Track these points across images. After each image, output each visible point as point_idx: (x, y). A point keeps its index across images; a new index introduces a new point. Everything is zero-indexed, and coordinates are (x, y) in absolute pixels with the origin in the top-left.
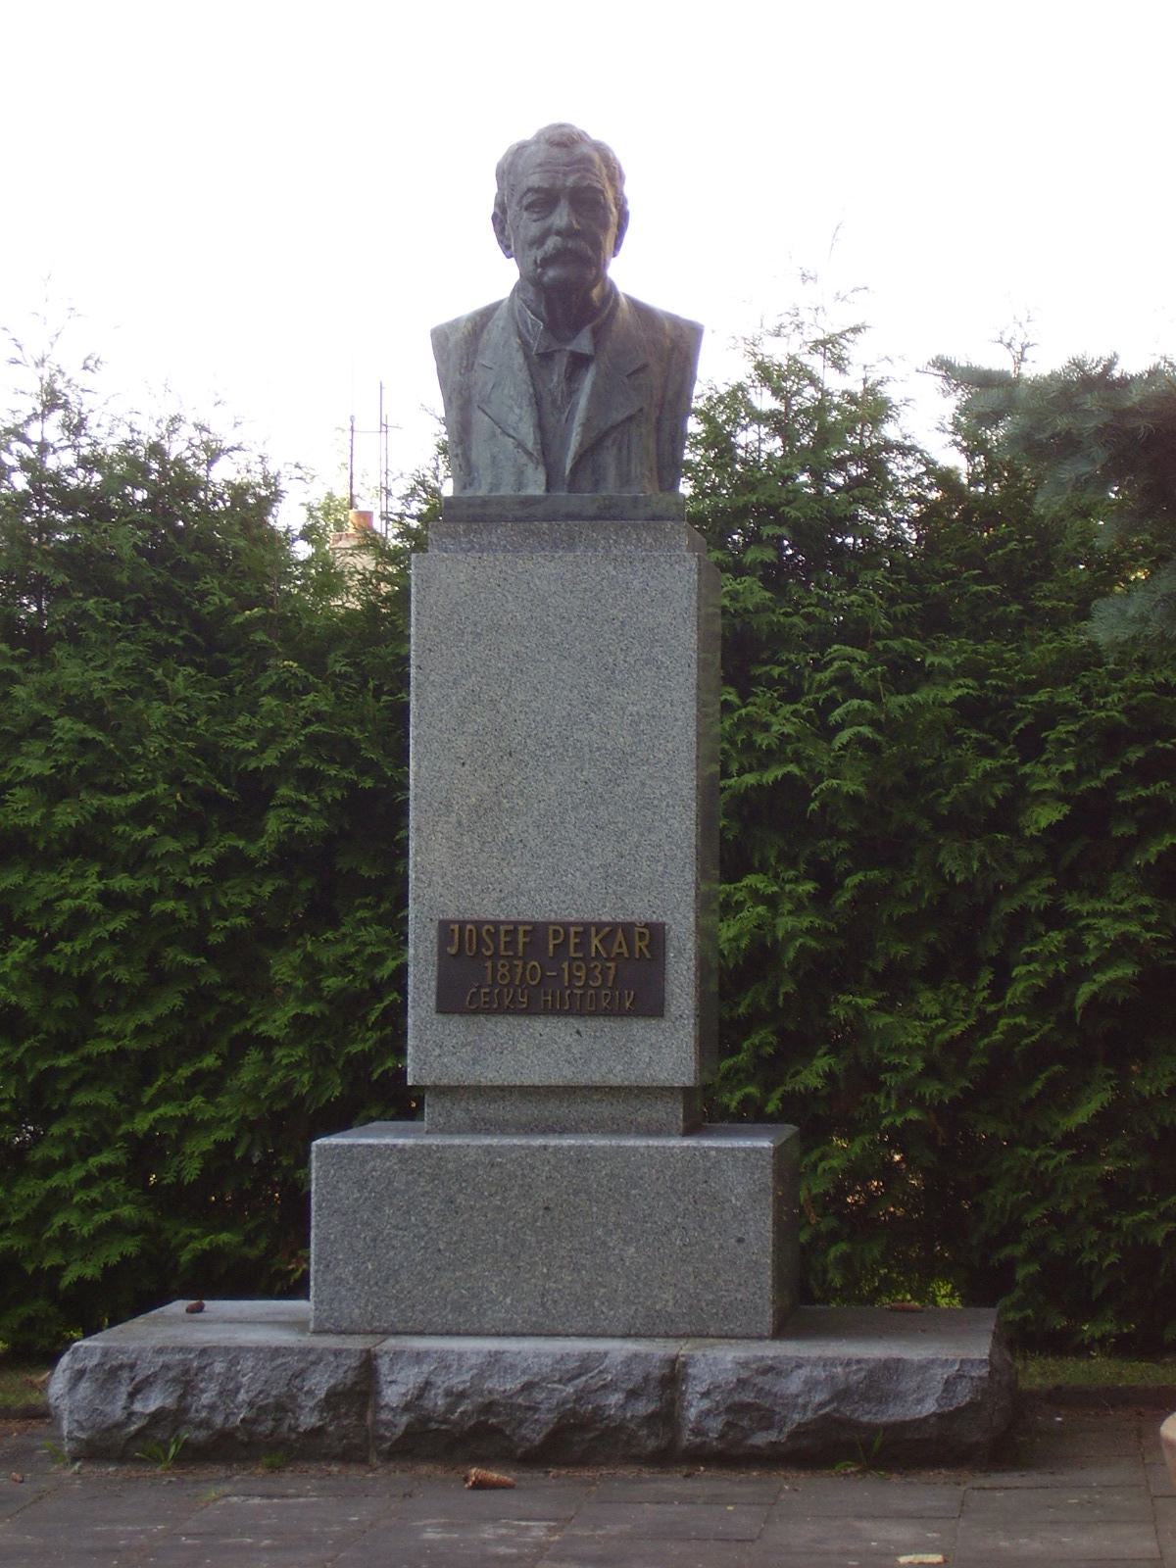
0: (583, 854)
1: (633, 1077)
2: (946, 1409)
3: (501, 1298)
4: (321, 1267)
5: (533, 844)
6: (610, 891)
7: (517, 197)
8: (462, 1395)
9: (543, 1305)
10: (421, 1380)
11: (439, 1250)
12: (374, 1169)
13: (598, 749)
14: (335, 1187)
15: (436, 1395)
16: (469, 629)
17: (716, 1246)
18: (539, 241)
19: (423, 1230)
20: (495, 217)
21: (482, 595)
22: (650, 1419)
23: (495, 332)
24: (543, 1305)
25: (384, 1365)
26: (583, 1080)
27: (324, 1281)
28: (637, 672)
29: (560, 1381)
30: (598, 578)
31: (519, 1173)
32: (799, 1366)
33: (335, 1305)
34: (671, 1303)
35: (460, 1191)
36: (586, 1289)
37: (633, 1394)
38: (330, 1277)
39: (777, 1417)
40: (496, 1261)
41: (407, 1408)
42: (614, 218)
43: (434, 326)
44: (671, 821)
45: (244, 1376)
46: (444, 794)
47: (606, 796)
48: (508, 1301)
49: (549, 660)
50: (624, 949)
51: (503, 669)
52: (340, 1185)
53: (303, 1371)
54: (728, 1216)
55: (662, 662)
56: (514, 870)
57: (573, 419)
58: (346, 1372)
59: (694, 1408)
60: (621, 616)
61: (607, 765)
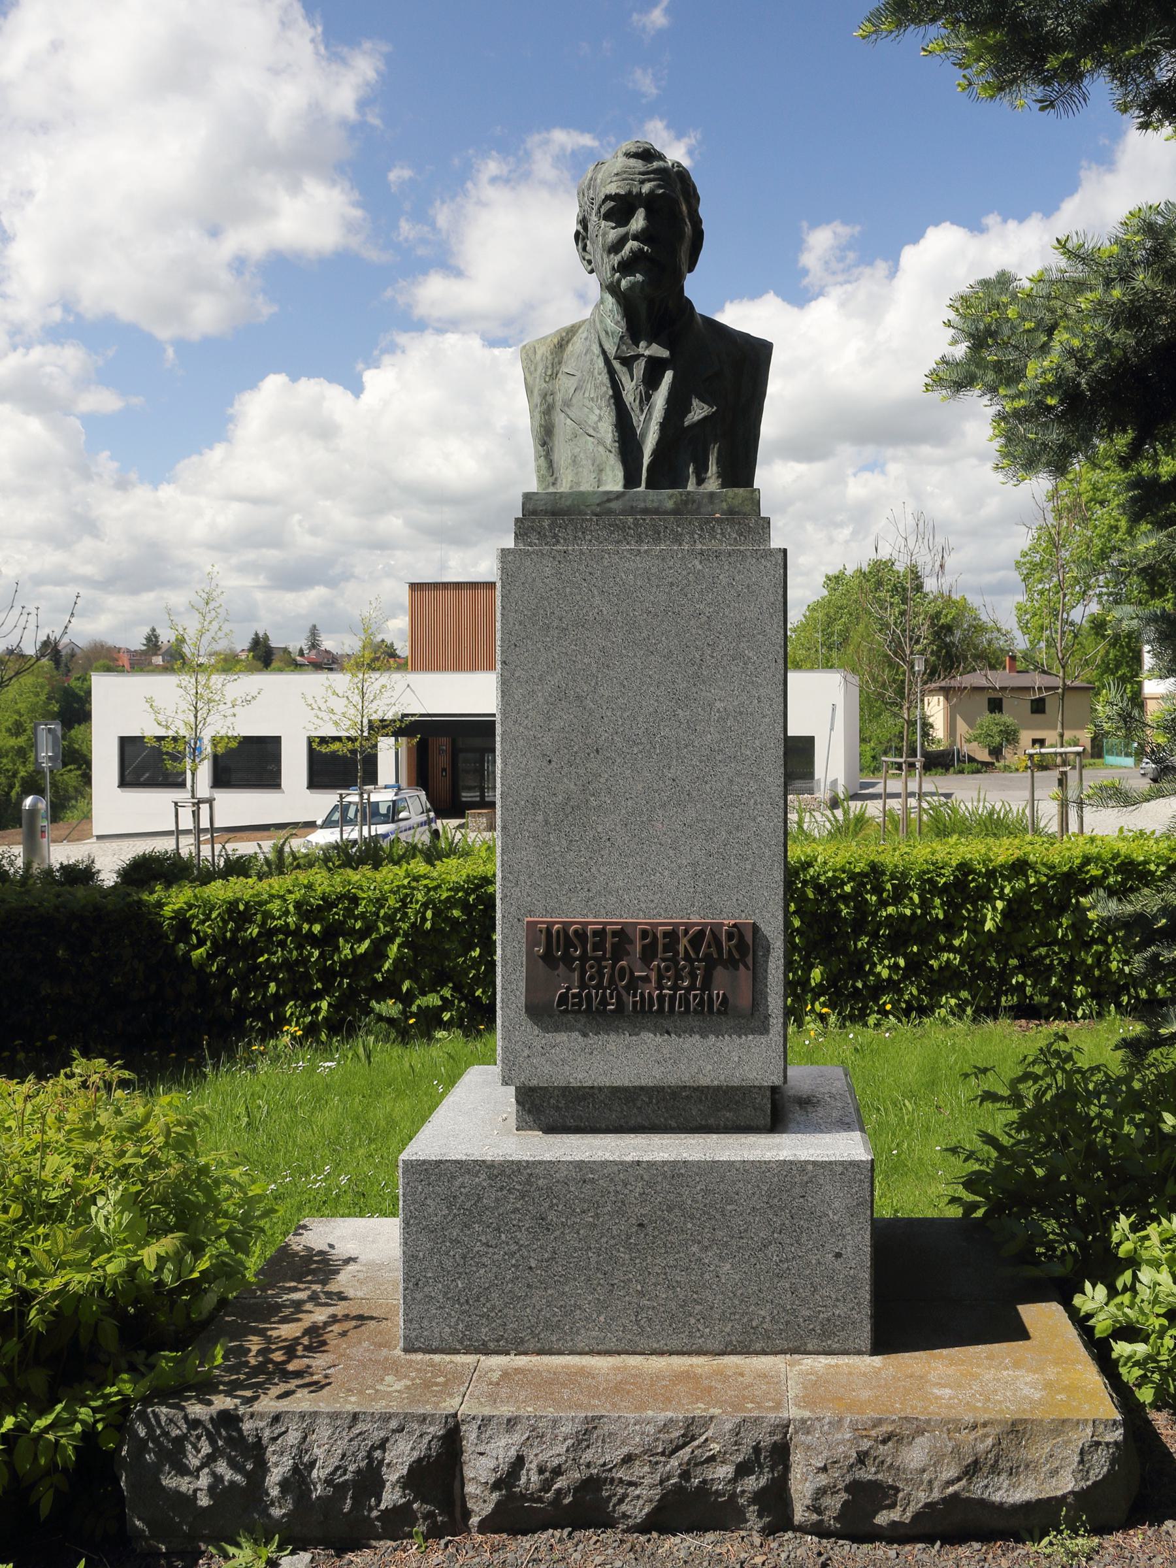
0: (671, 853)
3: (594, 1316)
4: (411, 1285)
5: (620, 842)
6: (699, 890)
7: (595, 207)
8: (557, 1471)
10: (513, 1453)
11: (531, 1268)
12: (462, 1186)
16: (555, 624)
17: (814, 1262)
18: (616, 248)
19: (514, 1248)
20: (577, 234)
21: (568, 590)
25: (470, 1434)
27: (414, 1299)
28: (724, 668)
29: (663, 1454)
30: (684, 573)
31: (612, 1189)
32: (920, 1432)
33: (425, 1323)
34: (768, 1319)
35: (551, 1207)
36: (681, 1306)
38: (419, 1296)
42: (688, 229)
45: (319, 1447)
47: (694, 794)
48: (602, 1319)
49: (635, 655)
51: (590, 664)
52: (428, 1202)
53: (386, 1440)
54: (824, 1230)
55: (749, 658)
56: (603, 870)
57: (650, 419)
58: (430, 1442)
60: (708, 610)
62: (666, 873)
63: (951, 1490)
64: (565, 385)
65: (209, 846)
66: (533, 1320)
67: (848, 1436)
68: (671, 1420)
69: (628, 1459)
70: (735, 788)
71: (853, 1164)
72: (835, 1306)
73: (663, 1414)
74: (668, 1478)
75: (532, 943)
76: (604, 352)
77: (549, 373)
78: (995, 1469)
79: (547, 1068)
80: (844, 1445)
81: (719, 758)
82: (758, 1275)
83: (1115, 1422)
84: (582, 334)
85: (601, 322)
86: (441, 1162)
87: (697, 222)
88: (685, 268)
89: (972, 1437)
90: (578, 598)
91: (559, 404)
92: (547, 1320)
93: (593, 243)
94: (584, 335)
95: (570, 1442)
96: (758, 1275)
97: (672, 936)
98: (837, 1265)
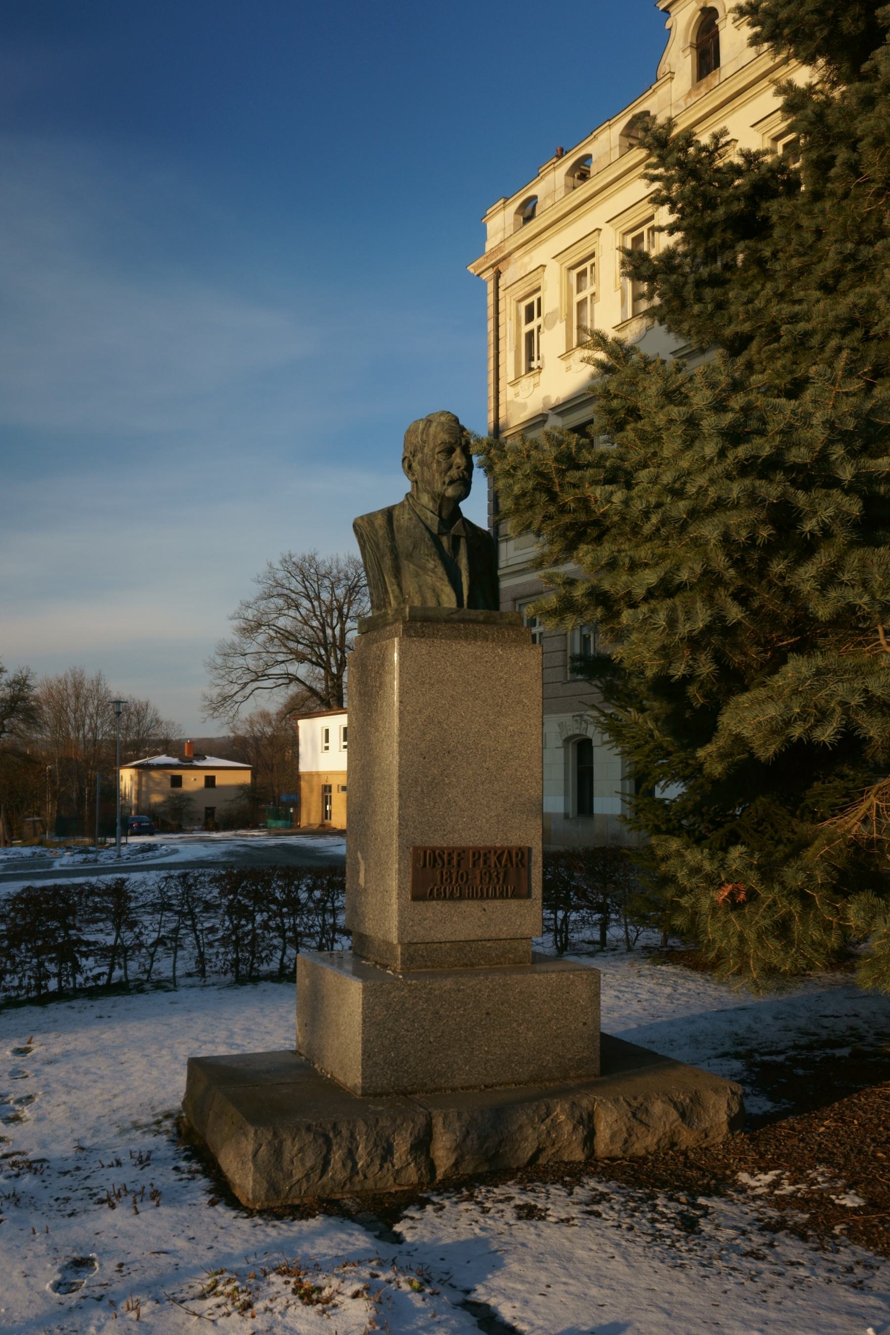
0: (486, 809)
9: (485, 1069)
14: (373, 1009)
19: (422, 1031)
24: (485, 1069)
33: (374, 1078)
35: (442, 1006)
38: (370, 1063)
48: (467, 1068)
61: (498, 759)
70: (518, 774)
75: (416, 860)
81: (511, 757)
82: (546, 1037)
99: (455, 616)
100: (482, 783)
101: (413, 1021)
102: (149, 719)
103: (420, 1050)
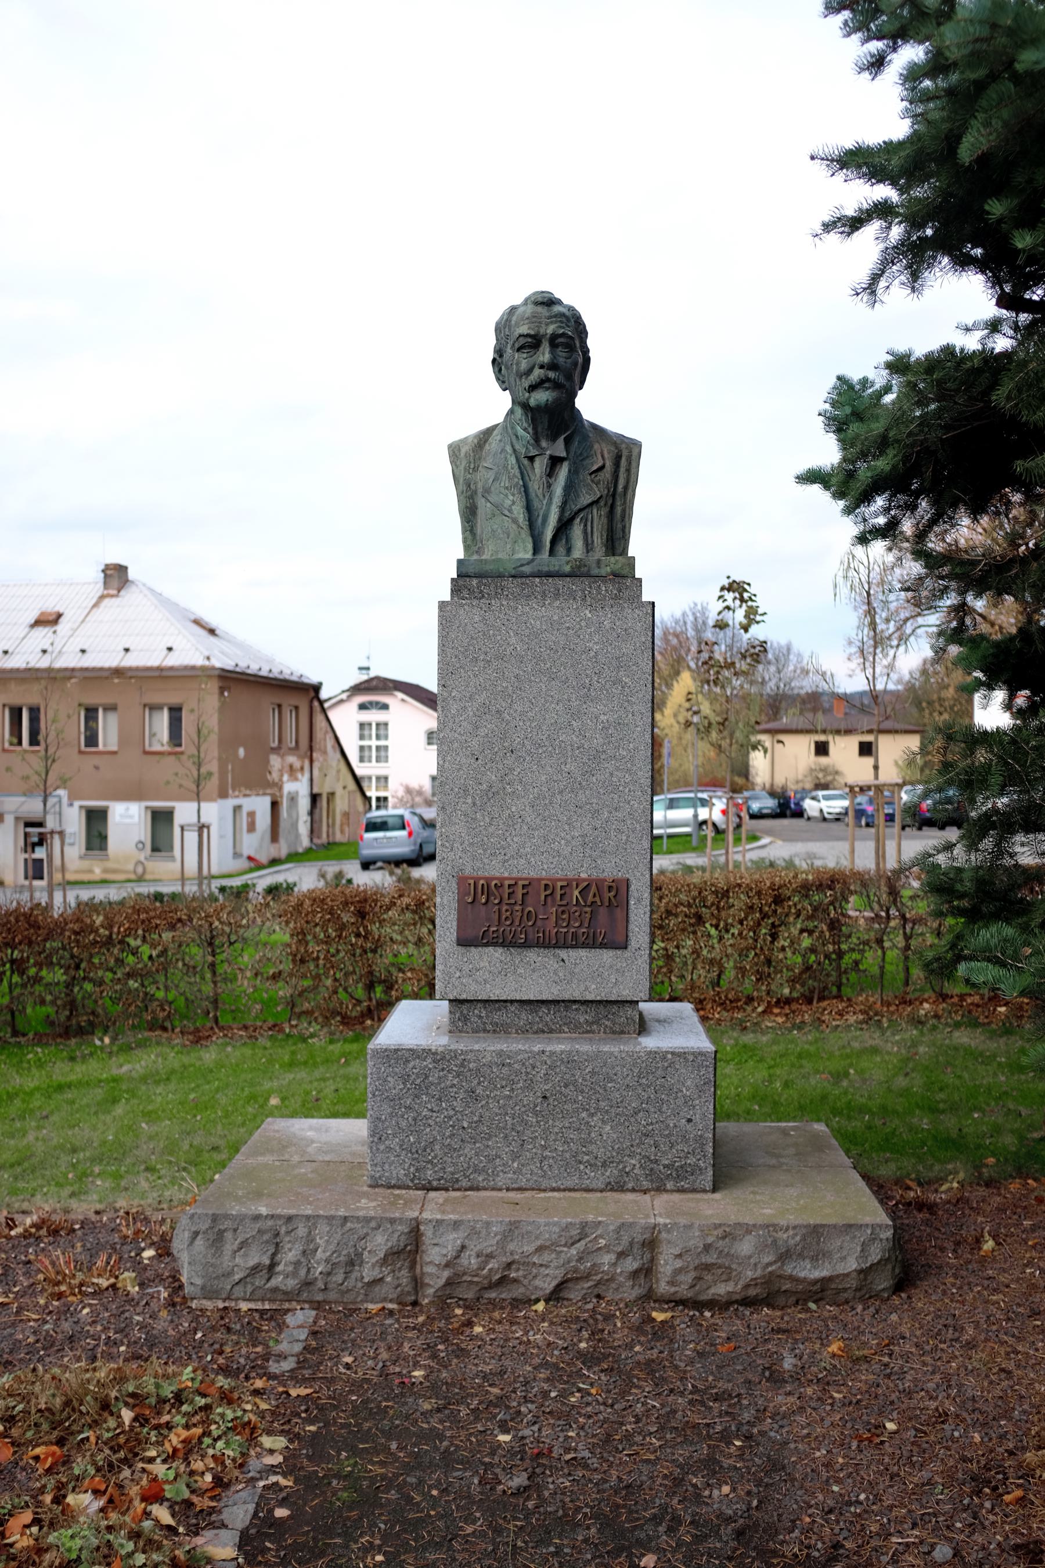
0: (567, 827)
1: (603, 995)
2: (864, 1266)
4: (376, 1139)
7: (510, 343)
8: (490, 1256)
9: (541, 1168)
12: (414, 1067)
13: (578, 748)
15: (470, 1256)
19: (452, 1113)
20: (494, 361)
22: (635, 1274)
23: (494, 444)
24: (541, 1168)
25: (427, 1230)
26: (567, 996)
29: (565, 1245)
33: (387, 1167)
34: (638, 1166)
35: (479, 1084)
37: (621, 1255)
38: (382, 1147)
39: (734, 1273)
40: (506, 1137)
41: (447, 1265)
43: (450, 442)
44: (632, 803)
46: (462, 781)
47: (584, 783)
48: (515, 1165)
50: (597, 899)
52: (389, 1079)
59: (667, 1264)
61: (585, 760)
62: (563, 842)
63: (770, 1269)
64: (484, 477)
65: (196, 834)
66: (465, 1165)
67: (697, 1234)
68: (571, 1223)
69: (540, 1249)
70: (614, 779)
71: (701, 1054)
72: (687, 1157)
73: (564, 1220)
74: (569, 1262)
76: (514, 451)
77: (472, 466)
78: (801, 1256)
79: (473, 987)
80: (695, 1242)
82: (631, 1135)
83: (887, 1226)
84: (496, 436)
85: (512, 428)
86: (398, 1050)
87: (586, 351)
88: (577, 387)
89: (785, 1236)
90: (499, 638)
91: (480, 491)
92: (475, 1166)
93: (507, 368)
94: (499, 437)
95: (499, 1237)
96: (631, 1135)
97: (568, 885)
98: (689, 1127)
99: (527, 569)
100: (561, 792)
101: (440, 1099)
102: (791, 668)
103: (450, 1137)
